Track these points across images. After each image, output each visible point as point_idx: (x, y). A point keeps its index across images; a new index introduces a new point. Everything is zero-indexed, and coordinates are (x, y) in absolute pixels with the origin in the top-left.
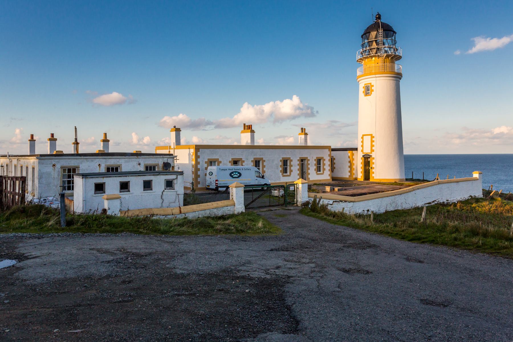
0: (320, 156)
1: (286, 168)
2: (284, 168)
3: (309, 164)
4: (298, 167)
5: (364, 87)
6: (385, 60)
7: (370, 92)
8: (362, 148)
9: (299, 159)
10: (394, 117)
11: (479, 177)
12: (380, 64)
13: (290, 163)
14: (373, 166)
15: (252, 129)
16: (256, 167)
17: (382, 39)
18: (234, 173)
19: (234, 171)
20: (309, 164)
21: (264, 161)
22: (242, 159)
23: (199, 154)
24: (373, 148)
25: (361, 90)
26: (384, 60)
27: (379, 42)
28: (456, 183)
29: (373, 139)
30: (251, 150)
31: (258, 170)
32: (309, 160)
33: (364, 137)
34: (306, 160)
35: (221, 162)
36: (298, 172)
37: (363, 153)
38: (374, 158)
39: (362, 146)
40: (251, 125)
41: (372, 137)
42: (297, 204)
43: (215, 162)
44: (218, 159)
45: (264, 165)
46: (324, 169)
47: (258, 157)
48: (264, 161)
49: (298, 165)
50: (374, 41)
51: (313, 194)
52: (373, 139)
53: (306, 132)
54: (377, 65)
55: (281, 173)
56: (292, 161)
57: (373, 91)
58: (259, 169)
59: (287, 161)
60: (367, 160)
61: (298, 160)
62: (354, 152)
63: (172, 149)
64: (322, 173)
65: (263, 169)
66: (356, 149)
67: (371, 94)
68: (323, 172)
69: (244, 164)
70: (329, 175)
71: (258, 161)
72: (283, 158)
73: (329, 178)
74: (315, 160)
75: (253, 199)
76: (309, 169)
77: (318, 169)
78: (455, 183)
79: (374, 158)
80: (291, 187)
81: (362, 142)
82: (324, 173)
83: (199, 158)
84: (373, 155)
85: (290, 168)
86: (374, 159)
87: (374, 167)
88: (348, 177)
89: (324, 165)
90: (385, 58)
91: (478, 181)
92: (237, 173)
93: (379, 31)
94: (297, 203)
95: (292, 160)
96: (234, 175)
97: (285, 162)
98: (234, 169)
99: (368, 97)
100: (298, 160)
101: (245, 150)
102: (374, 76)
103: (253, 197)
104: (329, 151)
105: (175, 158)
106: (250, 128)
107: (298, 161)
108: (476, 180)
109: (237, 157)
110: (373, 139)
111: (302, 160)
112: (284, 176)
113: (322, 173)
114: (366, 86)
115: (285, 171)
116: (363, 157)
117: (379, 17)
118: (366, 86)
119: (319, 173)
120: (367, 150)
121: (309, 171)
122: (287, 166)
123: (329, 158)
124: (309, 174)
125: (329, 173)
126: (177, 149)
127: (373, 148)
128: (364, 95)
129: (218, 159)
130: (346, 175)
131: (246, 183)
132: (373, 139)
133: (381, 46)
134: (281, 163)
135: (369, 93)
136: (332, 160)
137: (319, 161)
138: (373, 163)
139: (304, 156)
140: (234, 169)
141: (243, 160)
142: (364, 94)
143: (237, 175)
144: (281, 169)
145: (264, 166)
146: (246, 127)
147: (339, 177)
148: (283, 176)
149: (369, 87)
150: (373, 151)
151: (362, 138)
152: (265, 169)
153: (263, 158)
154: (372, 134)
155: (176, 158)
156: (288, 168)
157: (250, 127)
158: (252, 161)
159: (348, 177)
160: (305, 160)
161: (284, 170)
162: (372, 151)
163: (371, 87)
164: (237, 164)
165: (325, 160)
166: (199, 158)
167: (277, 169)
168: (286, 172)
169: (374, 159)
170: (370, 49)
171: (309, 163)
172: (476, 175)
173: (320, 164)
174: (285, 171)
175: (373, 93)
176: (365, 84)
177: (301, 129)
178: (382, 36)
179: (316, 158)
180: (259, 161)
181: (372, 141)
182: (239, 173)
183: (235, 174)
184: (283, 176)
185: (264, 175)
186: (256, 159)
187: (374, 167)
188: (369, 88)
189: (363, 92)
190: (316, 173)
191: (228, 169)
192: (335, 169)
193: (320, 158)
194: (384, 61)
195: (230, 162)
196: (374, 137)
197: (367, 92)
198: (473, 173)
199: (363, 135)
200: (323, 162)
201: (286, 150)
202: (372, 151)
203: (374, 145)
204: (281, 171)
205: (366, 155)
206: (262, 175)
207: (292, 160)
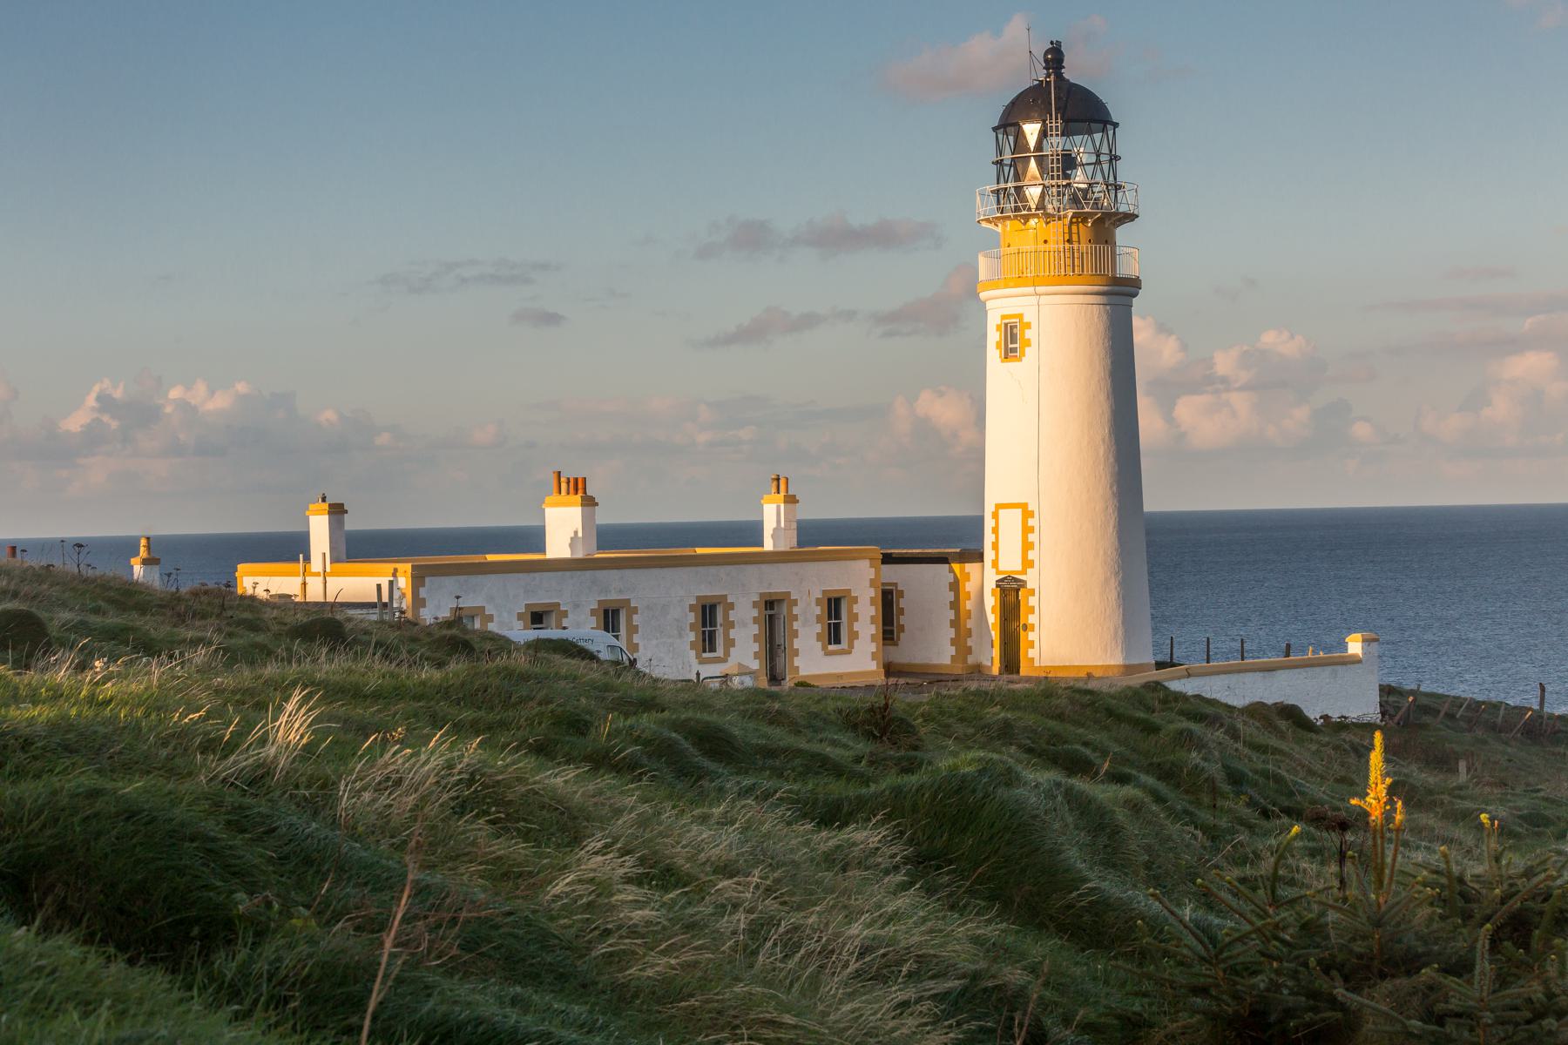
0: (836, 585)
2: (829, 624)
3: (795, 618)
4: (755, 629)
6: (1074, 228)
7: (1017, 345)
9: (596, 607)
10: (1103, 440)
11: (1364, 654)
12: (1057, 245)
13: (726, 616)
14: (1032, 619)
15: (585, 492)
16: (606, 629)
20: (795, 618)
21: (635, 611)
22: (559, 604)
23: (423, 593)
24: (1031, 555)
25: (994, 337)
26: (1070, 228)
28: (1261, 674)
29: (1031, 522)
30: (588, 574)
31: (614, 642)
32: (795, 603)
33: (1001, 512)
34: (554, 615)
36: (756, 647)
37: (998, 572)
38: (1032, 592)
39: (995, 546)
41: (1027, 514)
43: (473, 617)
44: (483, 608)
45: (731, 619)
46: (854, 636)
47: (614, 596)
48: (635, 611)
49: (755, 623)
50: (1032, 159)
53: (790, 493)
54: (1042, 247)
55: (693, 653)
56: (733, 609)
57: (1028, 342)
58: (617, 637)
59: (713, 607)
61: (755, 604)
63: (317, 574)
67: (1023, 354)
68: (851, 646)
69: (565, 623)
70: (874, 656)
71: (613, 611)
73: (872, 666)
74: (818, 602)
76: (795, 634)
77: (833, 635)
78: (1259, 675)
79: (1032, 592)
83: (424, 606)
84: (1031, 579)
85: (726, 635)
86: (1034, 595)
88: (947, 661)
89: (854, 618)
90: (1071, 222)
91: (1360, 665)
95: (732, 604)
99: (1012, 366)
100: (755, 604)
101: (568, 573)
102: (1030, 290)
104: (871, 567)
106: (580, 491)
108: (1355, 661)
109: (542, 599)
110: (1031, 522)
114: (1006, 325)
115: (708, 642)
116: (997, 586)
117: (1055, 59)
118: (1006, 325)
119: (831, 647)
120: (1010, 562)
121: (797, 644)
122: (715, 626)
123: (872, 593)
124: (796, 653)
125: (873, 648)
126: (333, 574)
127: (1031, 555)
129: (483, 608)
130: (942, 654)
136: (888, 601)
137: (834, 605)
138: (1032, 610)
139: (777, 588)
141: (562, 608)
144: (692, 636)
145: (633, 629)
146: (564, 486)
147: (917, 661)
149: (1016, 326)
152: (636, 639)
153: (629, 600)
156: (720, 631)
157: (580, 486)
158: (593, 612)
159: (947, 661)
160: (780, 601)
161: (704, 640)
162: (1027, 564)
163: (1022, 331)
164: (541, 622)
165: (855, 600)
167: (680, 636)
168: (713, 649)
169: (1034, 595)
171: (794, 613)
172: (1355, 646)
174: (708, 642)
175: (1027, 350)
176: (1003, 317)
180: (616, 612)
181: (1027, 530)
185: (635, 660)
186: (704, 602)
187: (1033, 625)
190: (824, 648)
192: (903, 631)
194: (1070, 233)
195: (520, 617)
196: (1032, 514)
197: (1010, 346)
199: (999, 506)
200: (850, 610)
201: (713, 570)
202: (1027, 564)
204: (693, 646)
205: (1005, 578)
206: (630, 659)
207: (732, 604)
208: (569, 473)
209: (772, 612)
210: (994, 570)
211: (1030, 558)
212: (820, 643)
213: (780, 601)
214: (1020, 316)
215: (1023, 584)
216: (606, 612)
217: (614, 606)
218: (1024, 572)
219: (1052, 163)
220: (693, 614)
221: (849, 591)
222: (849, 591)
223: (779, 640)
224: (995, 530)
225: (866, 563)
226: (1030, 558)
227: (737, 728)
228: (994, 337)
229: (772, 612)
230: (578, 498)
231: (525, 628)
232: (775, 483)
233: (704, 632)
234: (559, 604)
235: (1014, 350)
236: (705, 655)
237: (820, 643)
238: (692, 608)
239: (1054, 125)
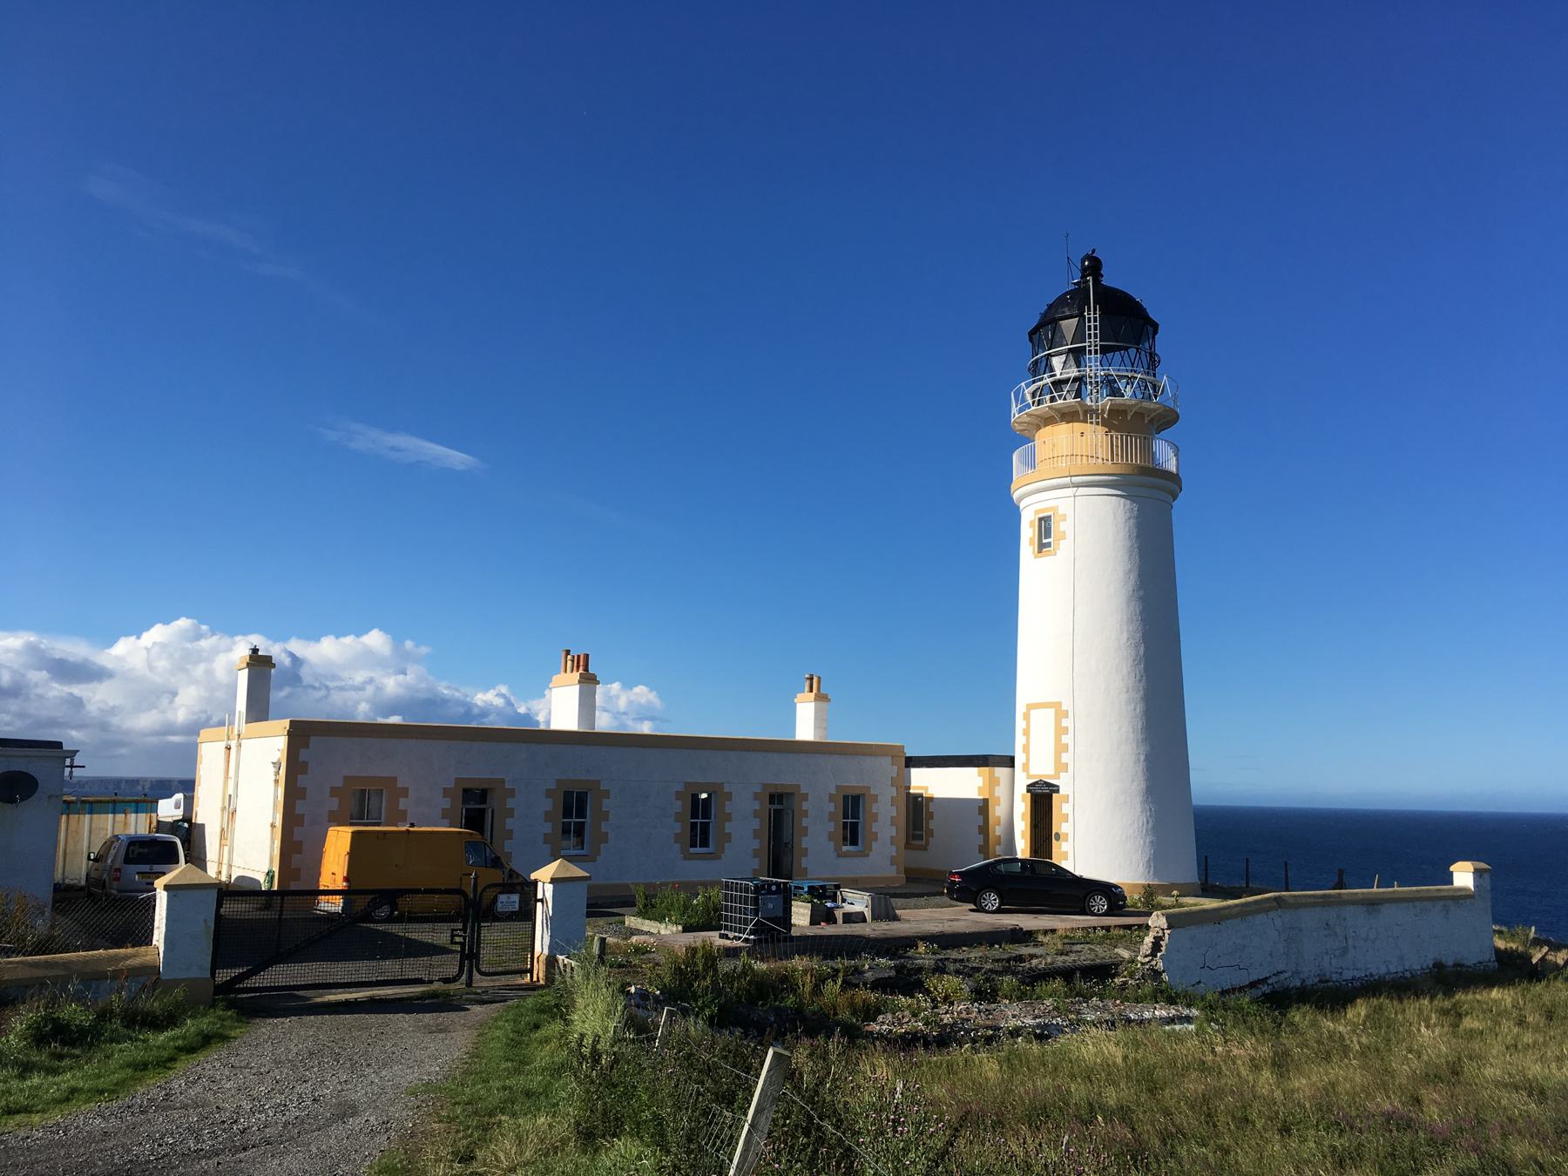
8: (1025, 755)
15: (586, 669)
17: (1096, 346)
22: (503, 781)
27: (1087, 349)
29: (1065, 723)
33: (1033, 712)
35: (404, 792)
37: (1029, 777)
38: (512, 793)
40: (587, 656)
52: (1063, 737)
55: (677, 847)
58: (482, 833)
60: (1042, 799)
61: (756, 796)
72: (558, 782)
84: (1064, 783)
87: (1067, 834)
93: (1086, 314)
99: (1046, 561)
105: (68, 762)
107: (445, 796)
108: (1462, 896)
116: (1028, 791)
128: (1034, 552)
132: (1063, 737)
135: (1050, 543)
142: (1031, 548)
150: (1065, 767)
154: (1060, 703)
155: (72, 760)
162: (1061, 767)
166: (305, 772)
168: (705, 844)
176: (1037, 512)
178: (1095, 335)
179: (833, 792)
181: (1060, 731)
187: (1067, 834)
192: (932, 836)
198: (1452, 869)
199: (1031, 707)
204: (831, 837)
205: (1036, 783)
209: (779, 807)
210: (1025, 774)
211: (1063, 761)
212: (832, 844)
215: (1055, 789)
216: (468, 794)
219: (1089, 330)
220: (679, 802)
223: (786, 838)
224: (1026, 732)
226: (1063, 761)
228: (1028, 532)
230: (576, 676)
232: (808, 682)
233: (694, 826)
234: (503, 781)
235: (1049, 545)
236: (692, 850)
237: (832, 844)
239: (1092, 316)
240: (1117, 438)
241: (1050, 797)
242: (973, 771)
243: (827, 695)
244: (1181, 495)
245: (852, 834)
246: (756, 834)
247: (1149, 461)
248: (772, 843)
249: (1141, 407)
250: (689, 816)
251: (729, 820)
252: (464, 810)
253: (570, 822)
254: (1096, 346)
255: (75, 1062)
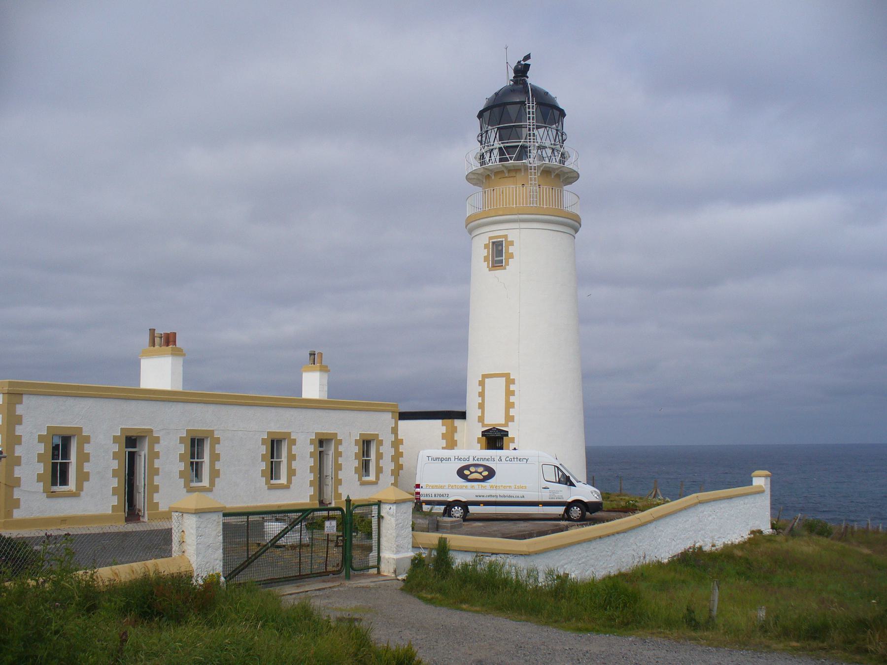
1: (64, 468)
5: (486, 246)
9: (185, 435)
11: (565, 506)
18: (472, 469)
19: (471, 462)
23: (20, 410)
24: (512, 412)
29: (512, 388)
32: (87, 439)
33: (487, 380)
37: (483, 426)
39: (481, 406)
41: (510, 381)
42: (379, 569)
51: (433, 538)
62: (458, 423)
64: (286, 483)
65: (83, 468)
66: (462, 415)
68: (80, 487)
75: (251, 553)
80: (327, 524)
81: (482, 395)
82: (291, 483)
89: (379, 456)
92: (480, 469)
93: (527, 103)
94: (378, 567)
96: (472, 473)
97: (275, 444)
98: (471, 459)
99: (498, 273)
100: (116, 439)
103: (248, 549)
110: (512, 388)
111: (322, 442)
112: (52, 495)
113: (286, 483)
115: (273, 472)
116: (483, 435)
117: (522, 71)
120: (495, 418)
127: (512, 412)
128: (488, 267)
131: (510, 496)
133: (532, 140)
134: (182, 449)
137: (366, 444)
140: (471, 459)
141: (155, 435)
143: (480, 473)
146: (157, 340)
148: (269, 489)
151: (482, 383)
162: (509, 419)
168: (64, 481)
170: (506, 148)
173: (368, 455)
174: (273, 472)
176: (490, 238)
177: (311, 354)
181: (509, 393)
182: (487, 468)
183: (476, 472)
184: (269, 489)
188: (500, 248)
189: (486, 259)
190: (360, 479)
191: (453, 459)
193: (369, 438)
196: (513, 382)
199: (485, 376)
200: (289, 450)
203: (513, 403)
208: (162, 330)
209: (321, 449)
213: (329, 441)
214: (506, 236)
215: (506, 434)
216: (193, 441)
217: (200, 436)
218: (506, 425)
221: (151, 431)
222: (80, 429)
225: (389, 415)
227: (622, 514)
229: (321, 449)
231: (481, 449)
233: (54, 465)
236: (55, 488)
238: (182, 440)
240: (546, 190)
241: (501, 438)
242: (439, 422)
243: (327, 367)
244: (580, 229)
245: (59, 474)
246: (115, 473)
247: (561, 206)
248: (333, 473)
249: (561, 171)
250: (190, 458)
251: (19, 464)
252: (127, 452)
253: (57, 463)
254: (533, 125)
255: (203, 577)
